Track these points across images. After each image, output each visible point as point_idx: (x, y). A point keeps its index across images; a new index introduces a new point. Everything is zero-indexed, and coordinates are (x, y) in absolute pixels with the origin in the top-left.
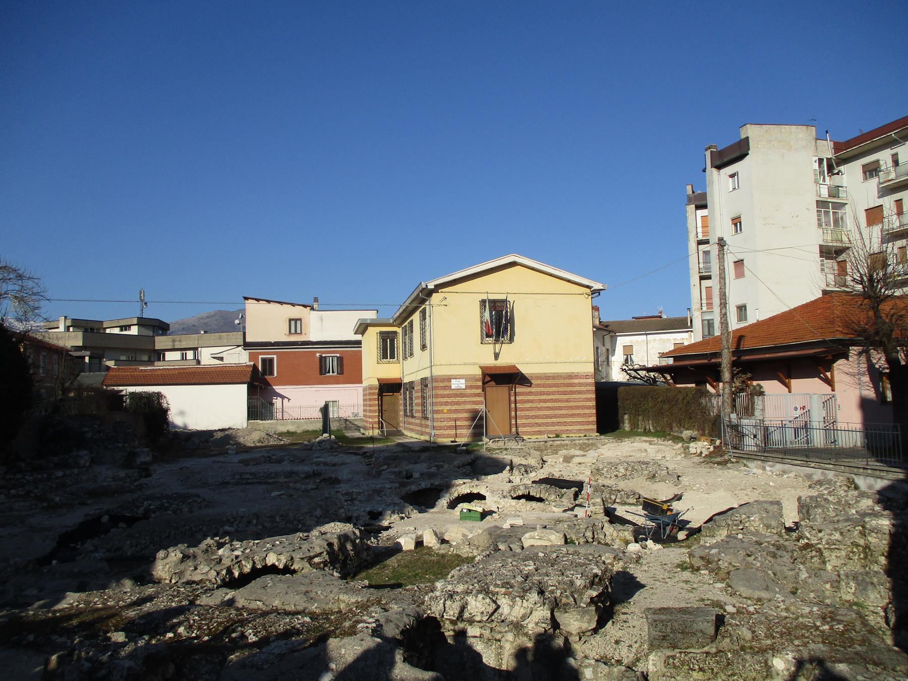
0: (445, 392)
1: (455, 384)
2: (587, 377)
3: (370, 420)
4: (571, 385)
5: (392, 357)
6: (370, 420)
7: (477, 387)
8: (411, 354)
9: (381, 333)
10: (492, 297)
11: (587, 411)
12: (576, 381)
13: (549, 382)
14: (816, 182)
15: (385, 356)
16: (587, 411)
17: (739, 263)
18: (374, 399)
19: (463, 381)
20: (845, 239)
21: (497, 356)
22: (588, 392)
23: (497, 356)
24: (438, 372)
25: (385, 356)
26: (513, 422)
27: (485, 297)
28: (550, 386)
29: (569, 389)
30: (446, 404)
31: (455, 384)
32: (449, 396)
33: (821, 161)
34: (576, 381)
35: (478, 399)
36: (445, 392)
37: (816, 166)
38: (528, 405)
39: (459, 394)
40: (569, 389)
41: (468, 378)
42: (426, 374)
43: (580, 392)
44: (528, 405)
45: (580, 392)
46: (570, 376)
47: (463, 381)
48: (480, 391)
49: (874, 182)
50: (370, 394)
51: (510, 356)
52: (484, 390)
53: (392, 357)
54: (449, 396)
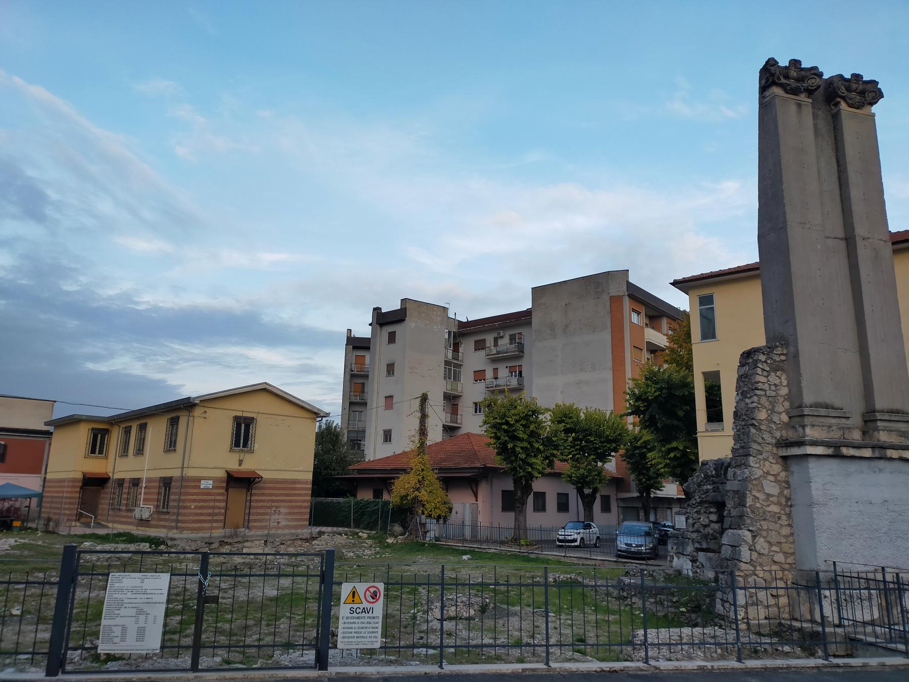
0: (195, 491)
1: (204, 484)
2: (306, 483)
3: (67, 512)
4: (294, 489)
5: (101, 452)
6: (67, 512)
7: (221, 488)
8: (140, 451)
9: (93, 429)
10: (245, 415)
11: (303, 510)
12: (298, 486)
13: (279, 486)
14: (446, 348)
15: (237, 444)
16: (303, 510)
17: (389, 398)
18: (76, 492)
19: (211, 482)
20: (459, 389)
21: (241, 462)
22: (306, 495)
23: (241, 462)
24: (191, 473)
25: (237, 444)
26: (247, 518)
27: (240, 414)
28: (279, 489)
29: (293, 492)
30: (194, 501)
31: (204, 484)
32: (197, 494)
33: (450, 333)
34: (298, 486)
35: (221, 498)
36: (195, 491)
37: (447, 336)
38: (260, 504)
39: (207, 492)
40: (293, 492)
41: (215, 480)
42: (176, 473)
43: (300, 495)
44: (260, 504)
45: (300, 495)
46: (295, 482)
47: (211, 482)
48: (223, 491)
49: (482, 353)
50: (73, 487)
51: (250, 463)
52: (227, 490)
53: (101, 452)
54: (197, 494)
